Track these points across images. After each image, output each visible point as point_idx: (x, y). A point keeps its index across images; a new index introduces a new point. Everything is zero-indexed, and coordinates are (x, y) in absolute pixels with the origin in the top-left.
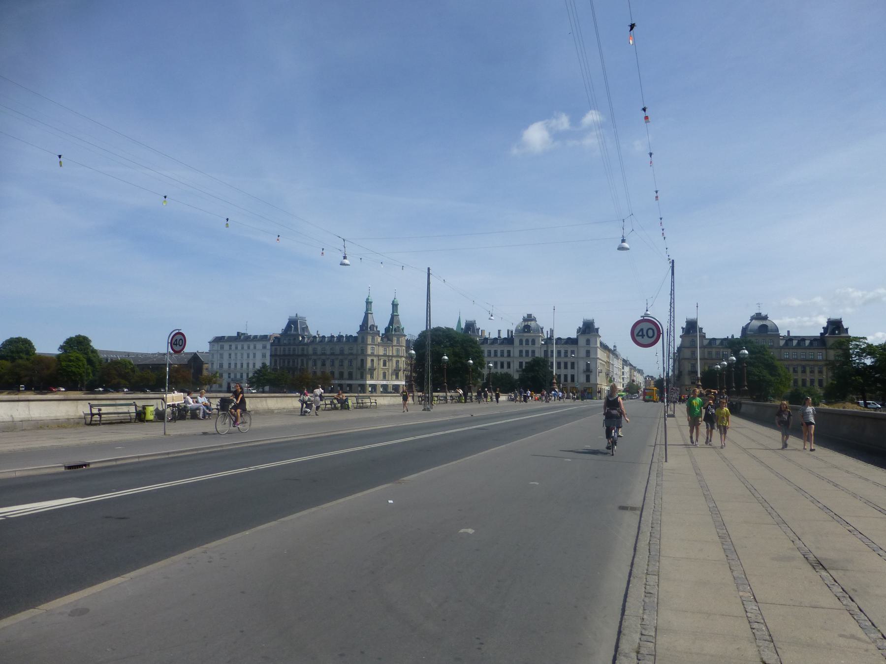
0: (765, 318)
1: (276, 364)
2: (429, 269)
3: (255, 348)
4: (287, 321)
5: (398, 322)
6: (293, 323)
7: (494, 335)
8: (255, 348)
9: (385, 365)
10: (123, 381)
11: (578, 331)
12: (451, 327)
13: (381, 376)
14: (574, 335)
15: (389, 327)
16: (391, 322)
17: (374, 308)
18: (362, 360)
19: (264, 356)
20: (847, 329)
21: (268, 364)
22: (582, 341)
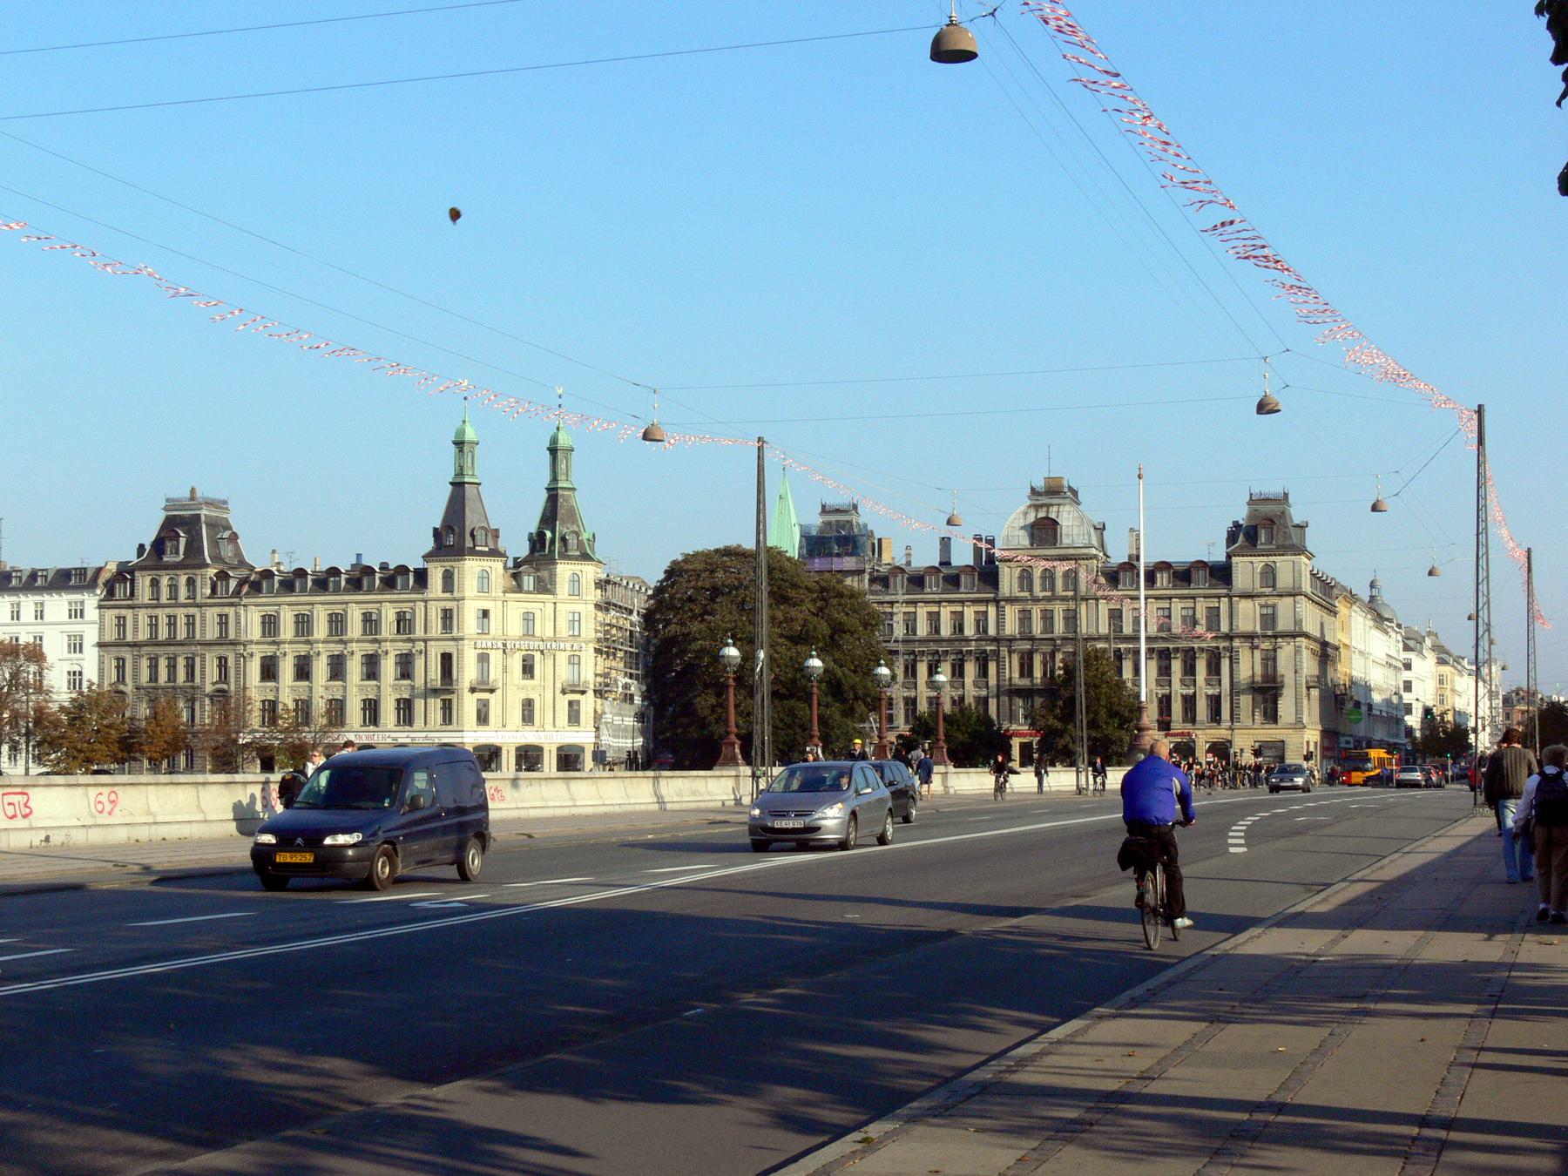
0: (1237, 525)
1: (121, 678)
2: (1480, 411)
3: (40, 615)
4: (160, 517)
5: (572, 516)
6: (1251, 502)
7: (926, 557)
8: (40, 615)
9: (528, 670)
10: (802, 648)
11: (1232, 538)
12: (731, 542)
13: (516, 714)
14: (1218, 555)
15: (541, 535)
16: (550, 516)
17: (481, 470)
18: (447, 659)
19: (76, 646)
20: (1301, 527)
21: (91, 674)
22: (1246, 570)
